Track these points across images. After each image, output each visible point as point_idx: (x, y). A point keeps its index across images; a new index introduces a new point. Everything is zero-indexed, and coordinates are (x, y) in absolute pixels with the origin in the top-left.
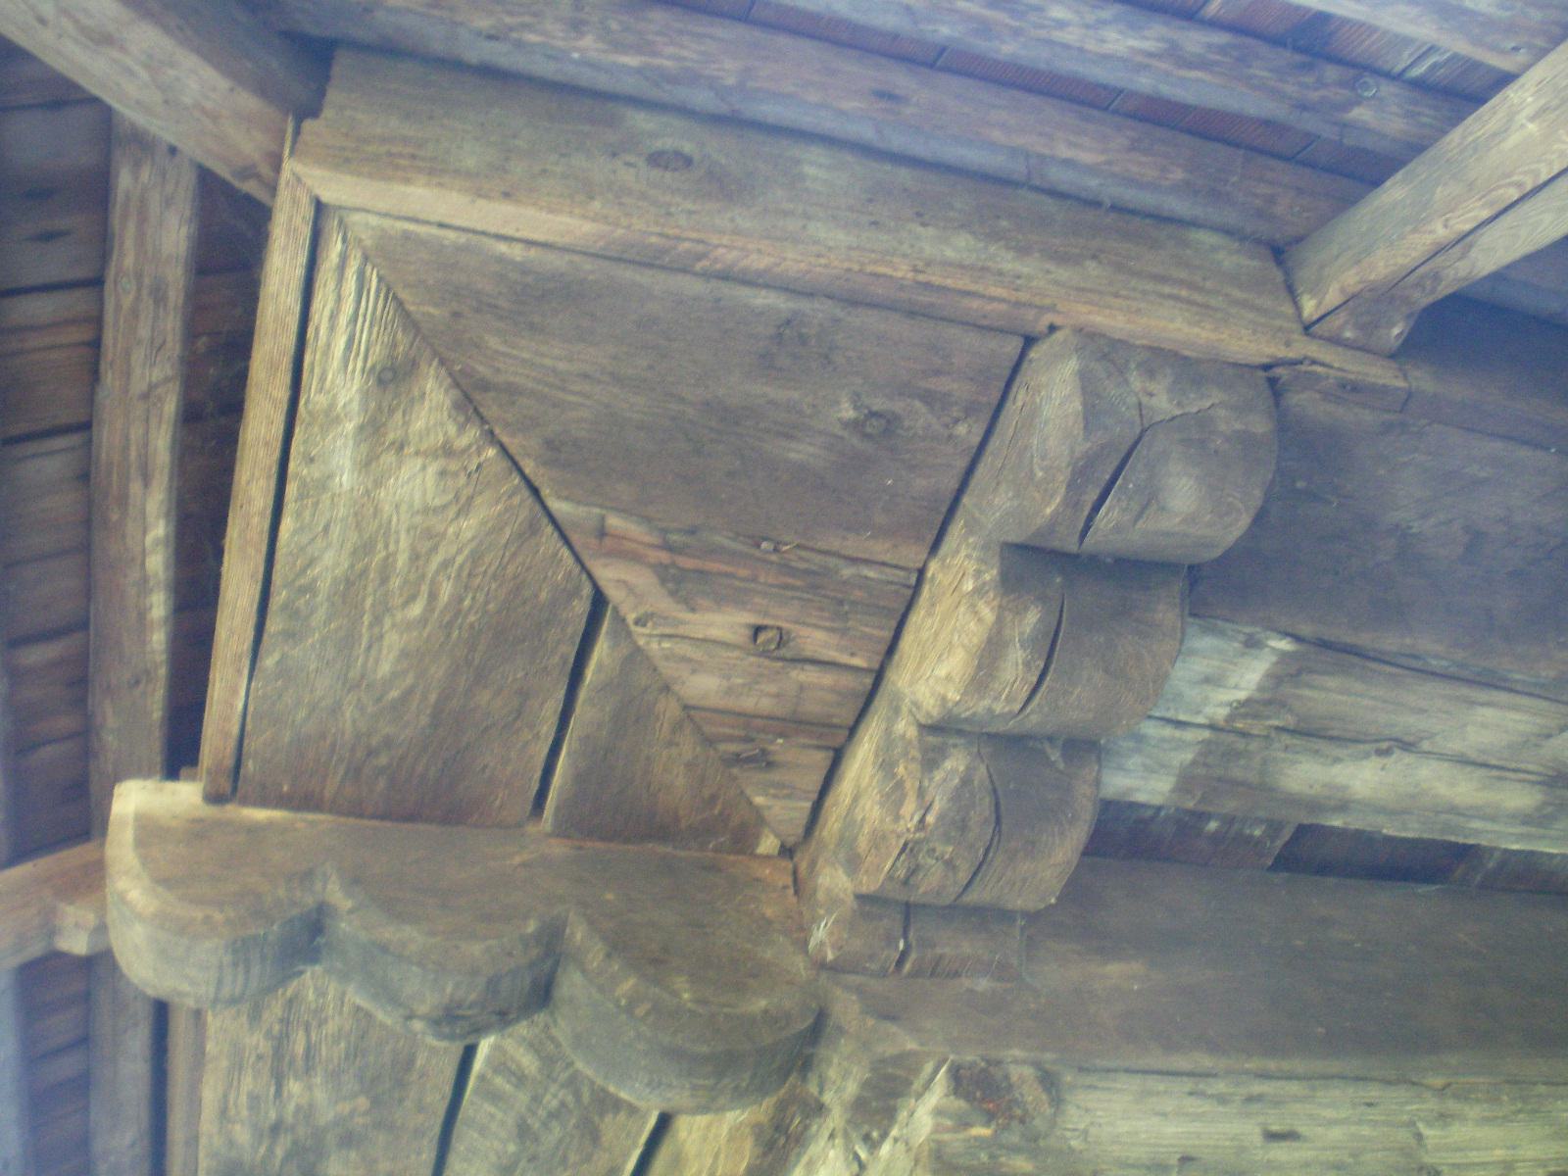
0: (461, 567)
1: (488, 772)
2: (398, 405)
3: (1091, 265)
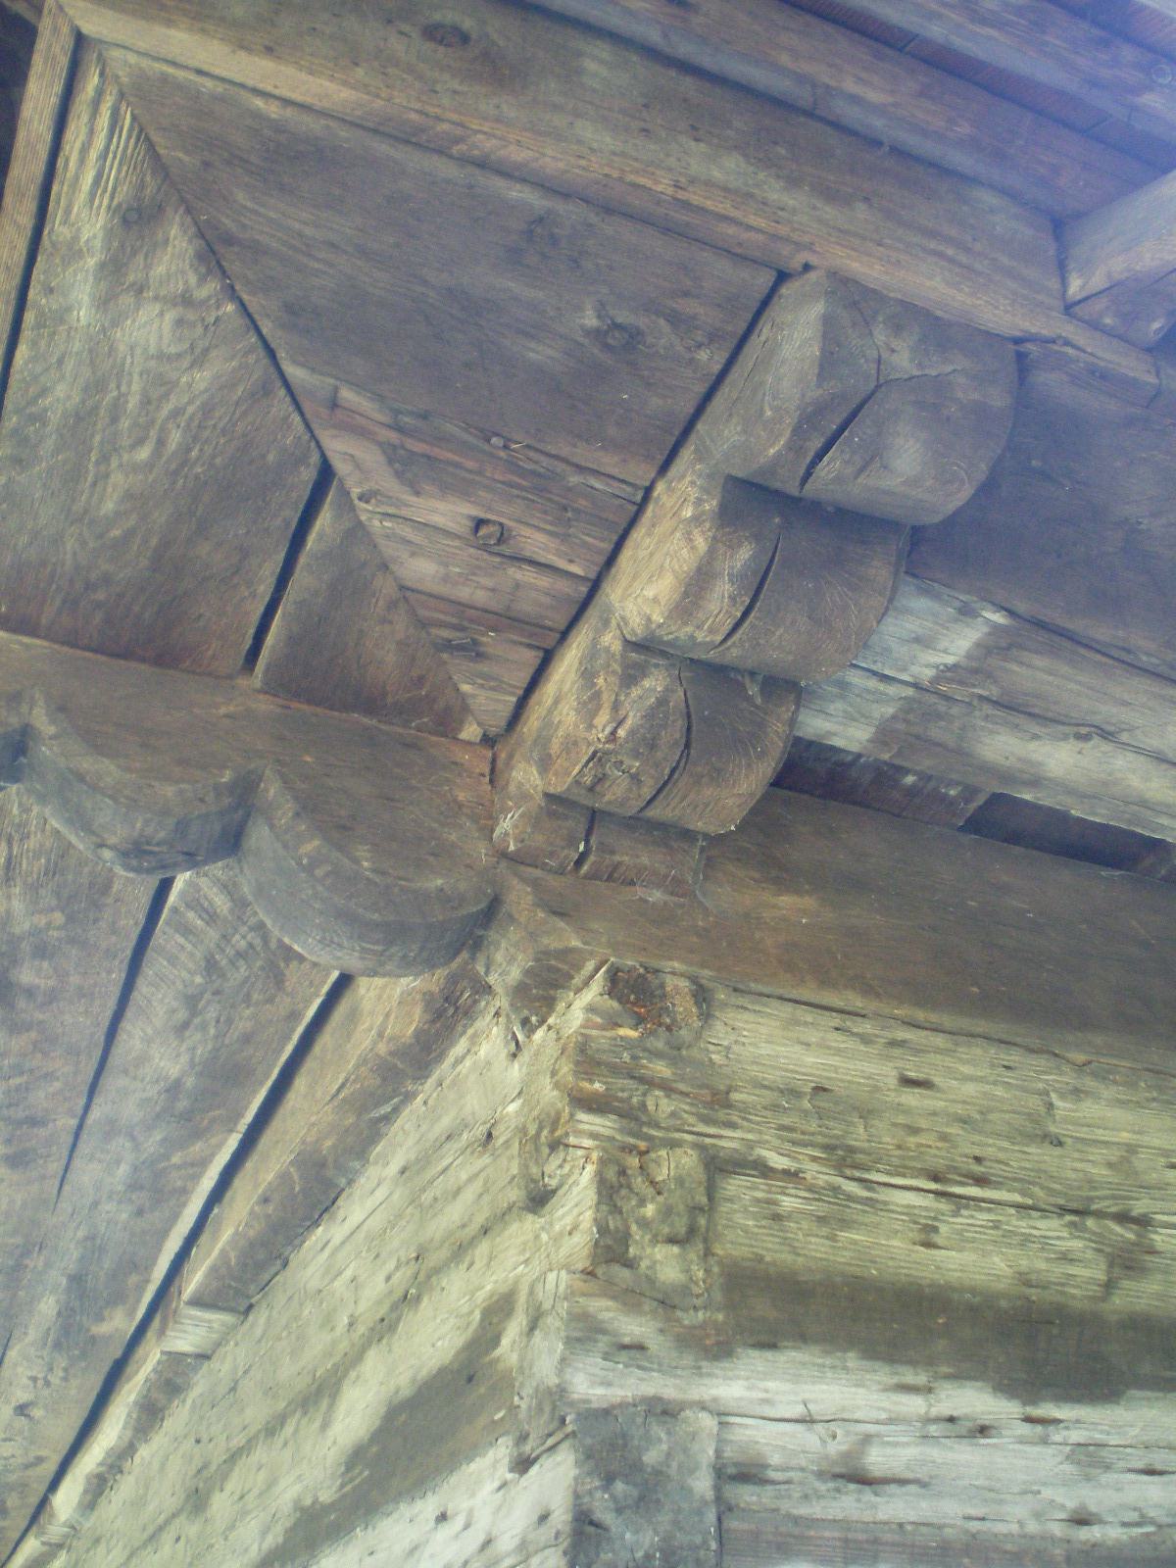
0: (191, 419)
1: (201, 624)
2: (141, 247)
3: (861, 206)
